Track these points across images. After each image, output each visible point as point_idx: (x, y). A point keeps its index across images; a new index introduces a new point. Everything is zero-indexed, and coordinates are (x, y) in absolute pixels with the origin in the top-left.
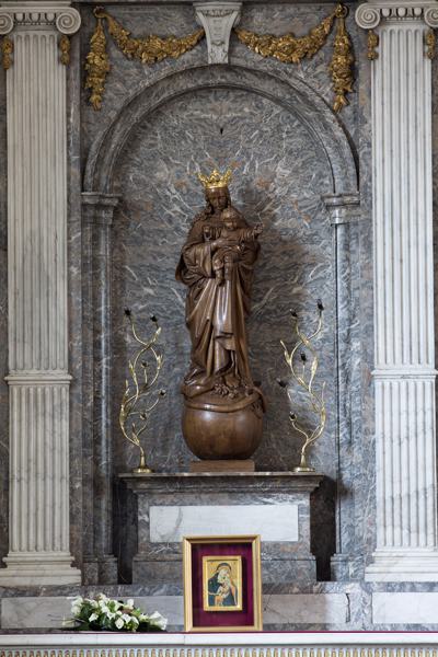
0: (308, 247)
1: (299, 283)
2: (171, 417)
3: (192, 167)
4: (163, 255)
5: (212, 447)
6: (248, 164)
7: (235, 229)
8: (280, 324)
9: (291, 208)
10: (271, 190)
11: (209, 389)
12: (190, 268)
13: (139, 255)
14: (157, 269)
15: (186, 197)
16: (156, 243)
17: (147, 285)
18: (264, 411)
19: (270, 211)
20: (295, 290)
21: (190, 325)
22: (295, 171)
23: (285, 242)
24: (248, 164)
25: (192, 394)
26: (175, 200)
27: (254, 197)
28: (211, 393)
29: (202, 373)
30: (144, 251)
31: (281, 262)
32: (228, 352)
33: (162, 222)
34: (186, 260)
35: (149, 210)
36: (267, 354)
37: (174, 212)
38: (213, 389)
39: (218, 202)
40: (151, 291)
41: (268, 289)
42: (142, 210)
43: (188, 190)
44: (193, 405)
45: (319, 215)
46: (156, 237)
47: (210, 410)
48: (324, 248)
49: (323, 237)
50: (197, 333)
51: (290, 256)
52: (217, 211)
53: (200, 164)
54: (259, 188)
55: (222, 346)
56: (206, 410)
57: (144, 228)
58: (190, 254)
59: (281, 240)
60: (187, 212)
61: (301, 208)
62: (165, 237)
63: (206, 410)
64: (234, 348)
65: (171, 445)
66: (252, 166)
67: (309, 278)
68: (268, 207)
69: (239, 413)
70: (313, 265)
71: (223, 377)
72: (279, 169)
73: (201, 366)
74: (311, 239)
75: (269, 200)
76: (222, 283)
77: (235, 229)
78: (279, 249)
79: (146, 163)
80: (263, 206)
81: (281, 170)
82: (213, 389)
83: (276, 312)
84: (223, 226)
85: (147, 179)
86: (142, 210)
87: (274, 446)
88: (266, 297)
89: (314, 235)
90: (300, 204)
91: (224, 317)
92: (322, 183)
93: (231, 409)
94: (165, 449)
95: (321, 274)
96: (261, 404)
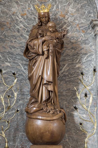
0: (83, 46)
1: (79, 62)
2: (17, 125)
3: (29, 6)
4: (15, 47)
5: (42, 138)
6: (55, 6)
7: (54, 32)
8: (70, 81)
9: (76, 27)
10: (66, 18)
11: (40, 110)
12: (32, 50)
13: (3, 47)
14: (12, 54)
15: (26, 21)
16: (11, 42)
17: (7, 61)
18: (65, 121)
19: (66, 28)
20: (77, 66)
21: (30, 78)
22: (78, 10)
23: (73, 43)
24: (55, 6)
25: (32, 112)
26: (21, 22)
27: (58, 22)
28: (41, 111)
29: (36, 102)
30: (6, 45)
31: (71, 52)
32: (49, 91)
33: (15, 32)
34: (29, 47)
35: (9, 26)
36: (64, 95)
37: (21, 27)
38: (42, 109)
39: (44, 20)
40: (9, 64)
41: (64, 65)
42: (5, 25)
43: (27, 17)
44: (33, 117)
45: (89, 31)
46: (12, 39)
47: (41, 119)
48: (91, 46)
49: (90, 41)
50: (34, 82)
51: (75, 50)
52: (43, 24)
53: (33, 5)
54: (61, 18)
55: (46, 88)
56: (39, 119)
57: (6, 34)
58: (32, 44)
59: (70, 42)
60: (26, 27)
61: (80, 27)
62: (16, 39)
63: (39, 119)
64: (52, 90)
65: (17, 139)
66: (57, 7)
67: (84, 60)
68: (65, 26)
69: (55, 121)
70: (86, 54)
71: (46, 104)
72: (70, 9)
73: (36, 99)
74: (85, 42)
75: (65, 23)
76: (48, 58)
77: (54, 32)
78: (70, 46)
79: (7, 3)
80: (62, 26)
81: (71, 9)
82: (42, 109)
83: (68, 76)
84: (48, 30)
85: (8, 11)
86: (5, 25)
87: (67, 140)
88: (64, 69)
89: (87, 40)
90: (80, 26)
91: (49, 73)
92: (90, 16)
93: (52, 119)
94: (14, 141)
95: (89, 59)
96: (64, 118)
